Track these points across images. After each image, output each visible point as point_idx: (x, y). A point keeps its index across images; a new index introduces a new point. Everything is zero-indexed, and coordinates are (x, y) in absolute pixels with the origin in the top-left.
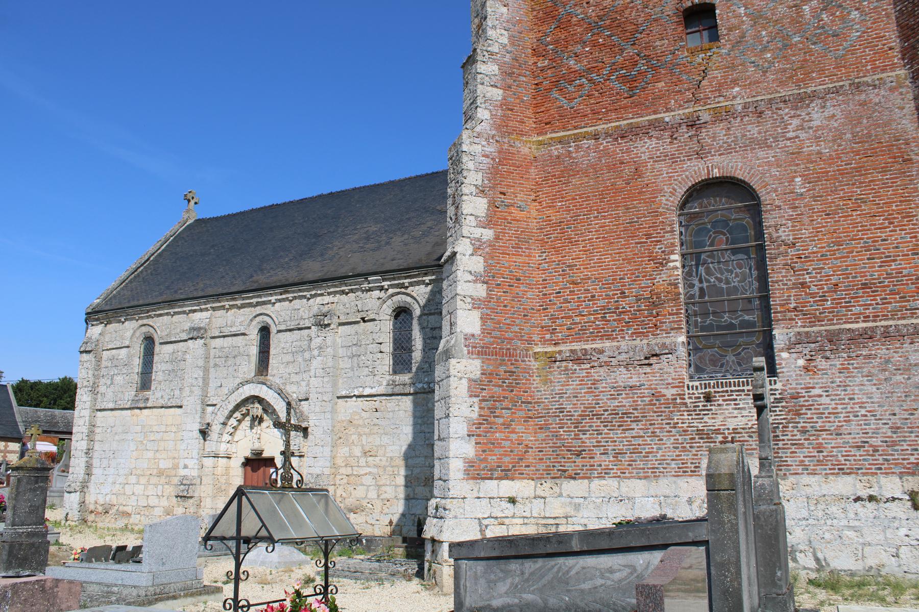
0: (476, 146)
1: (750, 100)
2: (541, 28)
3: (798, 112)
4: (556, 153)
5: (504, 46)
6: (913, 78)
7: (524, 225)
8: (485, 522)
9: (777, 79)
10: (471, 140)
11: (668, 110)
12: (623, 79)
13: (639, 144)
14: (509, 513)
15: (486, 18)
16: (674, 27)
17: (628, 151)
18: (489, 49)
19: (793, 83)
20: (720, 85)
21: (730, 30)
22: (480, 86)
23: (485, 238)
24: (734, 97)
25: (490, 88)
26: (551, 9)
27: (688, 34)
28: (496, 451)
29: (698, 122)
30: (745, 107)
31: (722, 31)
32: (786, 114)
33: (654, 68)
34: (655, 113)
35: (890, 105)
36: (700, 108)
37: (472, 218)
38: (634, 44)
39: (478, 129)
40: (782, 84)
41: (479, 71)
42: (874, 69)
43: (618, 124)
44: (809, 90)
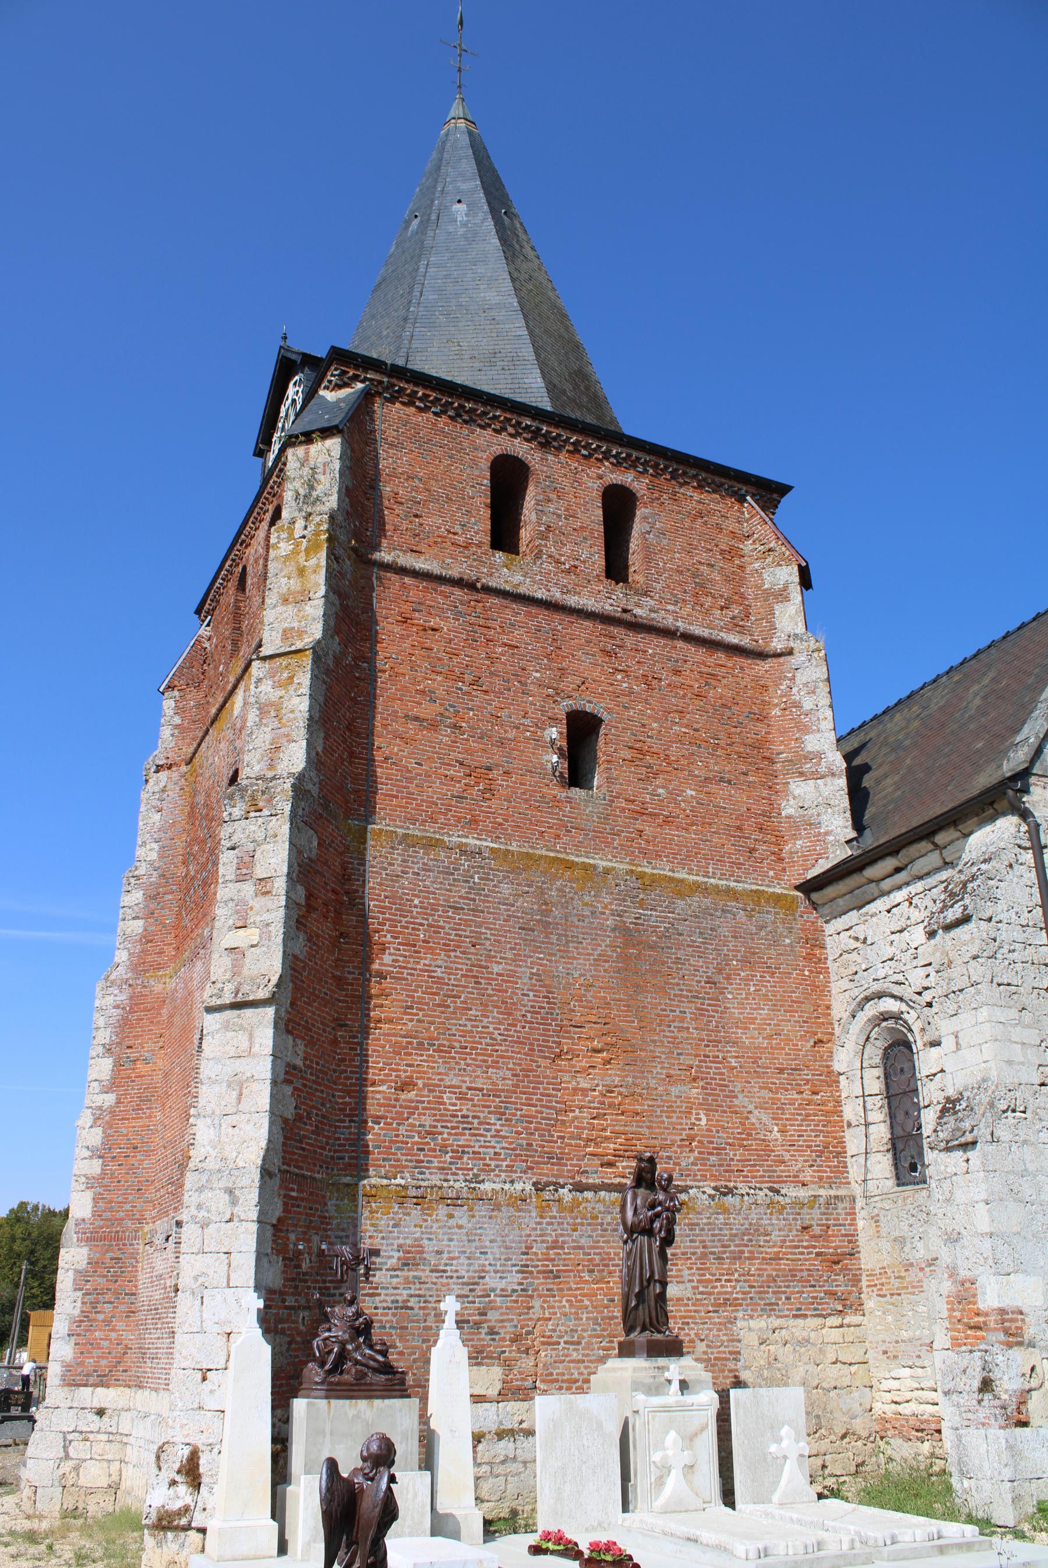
5: (151, 863)
7: (147, 1080)
8: (70, 1437)
14: (94, 1427)
23: (107, 1104)
28: (96, 1353)
37: (96, 1084)
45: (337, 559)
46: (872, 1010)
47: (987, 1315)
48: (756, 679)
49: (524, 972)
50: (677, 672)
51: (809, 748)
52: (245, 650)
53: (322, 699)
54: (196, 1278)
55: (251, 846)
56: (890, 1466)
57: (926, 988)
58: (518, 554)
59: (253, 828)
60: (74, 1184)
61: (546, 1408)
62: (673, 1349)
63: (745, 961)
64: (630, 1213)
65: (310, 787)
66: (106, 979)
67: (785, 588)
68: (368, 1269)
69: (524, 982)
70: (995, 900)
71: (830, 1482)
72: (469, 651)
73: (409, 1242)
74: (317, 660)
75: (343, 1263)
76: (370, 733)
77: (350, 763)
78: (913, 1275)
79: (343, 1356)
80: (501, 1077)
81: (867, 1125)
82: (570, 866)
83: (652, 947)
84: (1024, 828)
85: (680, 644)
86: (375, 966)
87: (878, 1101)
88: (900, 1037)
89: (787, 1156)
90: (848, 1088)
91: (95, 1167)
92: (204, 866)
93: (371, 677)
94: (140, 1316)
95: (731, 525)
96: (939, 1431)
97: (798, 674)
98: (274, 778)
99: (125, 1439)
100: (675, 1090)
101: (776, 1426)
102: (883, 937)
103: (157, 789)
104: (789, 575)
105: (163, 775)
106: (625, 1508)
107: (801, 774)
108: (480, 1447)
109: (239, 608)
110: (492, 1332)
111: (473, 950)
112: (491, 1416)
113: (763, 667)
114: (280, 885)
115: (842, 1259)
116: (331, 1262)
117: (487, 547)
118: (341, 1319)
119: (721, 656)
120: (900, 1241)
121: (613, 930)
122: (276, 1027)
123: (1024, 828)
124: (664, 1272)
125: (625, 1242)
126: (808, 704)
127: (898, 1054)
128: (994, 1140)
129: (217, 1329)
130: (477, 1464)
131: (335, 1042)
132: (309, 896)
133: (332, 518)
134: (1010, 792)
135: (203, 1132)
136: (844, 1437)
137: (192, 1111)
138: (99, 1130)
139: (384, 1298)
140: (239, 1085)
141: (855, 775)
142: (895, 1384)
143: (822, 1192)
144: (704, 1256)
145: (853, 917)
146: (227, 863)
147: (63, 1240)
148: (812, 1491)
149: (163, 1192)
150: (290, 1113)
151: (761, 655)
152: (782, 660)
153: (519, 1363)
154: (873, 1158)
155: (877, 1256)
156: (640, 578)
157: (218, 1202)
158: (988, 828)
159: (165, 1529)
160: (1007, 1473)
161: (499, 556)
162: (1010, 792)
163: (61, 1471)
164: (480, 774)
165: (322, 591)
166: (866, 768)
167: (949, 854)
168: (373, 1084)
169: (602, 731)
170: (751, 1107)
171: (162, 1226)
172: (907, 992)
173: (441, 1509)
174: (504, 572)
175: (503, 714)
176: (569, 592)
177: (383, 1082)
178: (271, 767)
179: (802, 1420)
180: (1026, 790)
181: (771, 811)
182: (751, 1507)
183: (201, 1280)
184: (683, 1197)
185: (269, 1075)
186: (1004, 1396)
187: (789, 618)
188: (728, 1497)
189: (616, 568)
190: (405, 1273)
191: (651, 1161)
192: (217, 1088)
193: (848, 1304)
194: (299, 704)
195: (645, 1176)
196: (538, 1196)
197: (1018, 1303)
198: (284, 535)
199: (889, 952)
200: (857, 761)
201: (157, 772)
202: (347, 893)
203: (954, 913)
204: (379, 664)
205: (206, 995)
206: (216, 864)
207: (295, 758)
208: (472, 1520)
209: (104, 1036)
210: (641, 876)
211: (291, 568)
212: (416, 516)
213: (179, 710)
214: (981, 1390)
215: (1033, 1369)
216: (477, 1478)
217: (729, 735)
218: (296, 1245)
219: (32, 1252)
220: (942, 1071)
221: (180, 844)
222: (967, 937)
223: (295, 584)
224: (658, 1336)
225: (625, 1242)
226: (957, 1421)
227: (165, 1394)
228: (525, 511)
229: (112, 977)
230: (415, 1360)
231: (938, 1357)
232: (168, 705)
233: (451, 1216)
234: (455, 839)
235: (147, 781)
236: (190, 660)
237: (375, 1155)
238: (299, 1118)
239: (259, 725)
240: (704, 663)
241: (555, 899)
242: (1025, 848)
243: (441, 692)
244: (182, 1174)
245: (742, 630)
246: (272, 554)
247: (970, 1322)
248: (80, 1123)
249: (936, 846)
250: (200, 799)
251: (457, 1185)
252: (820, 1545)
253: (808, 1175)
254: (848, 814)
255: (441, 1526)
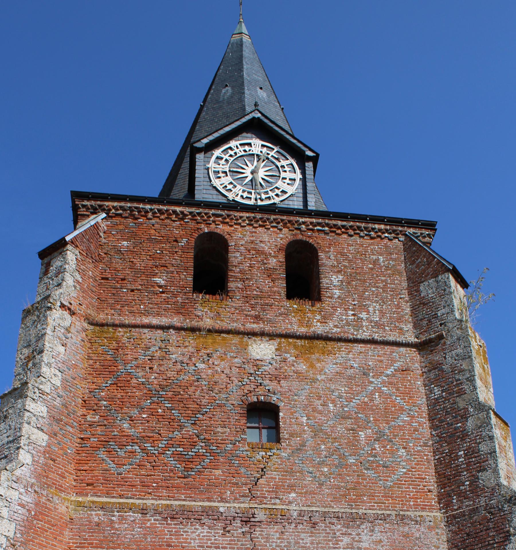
0: (13, 492)
1: (305, 508)
2: (95, 380)
3: (349, 531)
4: (96, 519)
6: (447, 522)
9: (332, 494)
10: (10, 484)
11: (223, 500)
12: (179, 457)
13: (189, 528)
15: (41, 352)
16: (237, 417)
17: (177, 534)
18: (41, 387)
19: (346, 501)
20: (277, 487)
21: (292, 435)
22: (25, 425)
24: (290, 503)
25: (36, 431)
26: (110, 363)
27: (248, 428)
29: (253, 520)
30: (300, 515)
31: (284, 434)
32: (338, 531)
33: (212, 453)
34: (209, 500)
35: (427, 542)
36: (256, 506)
38: (195, 424)
39: (18, 472)
40: (336, 500)
41: (27, 407)
42: (416, 505)
43: (168, 502)
44: (361, 512)
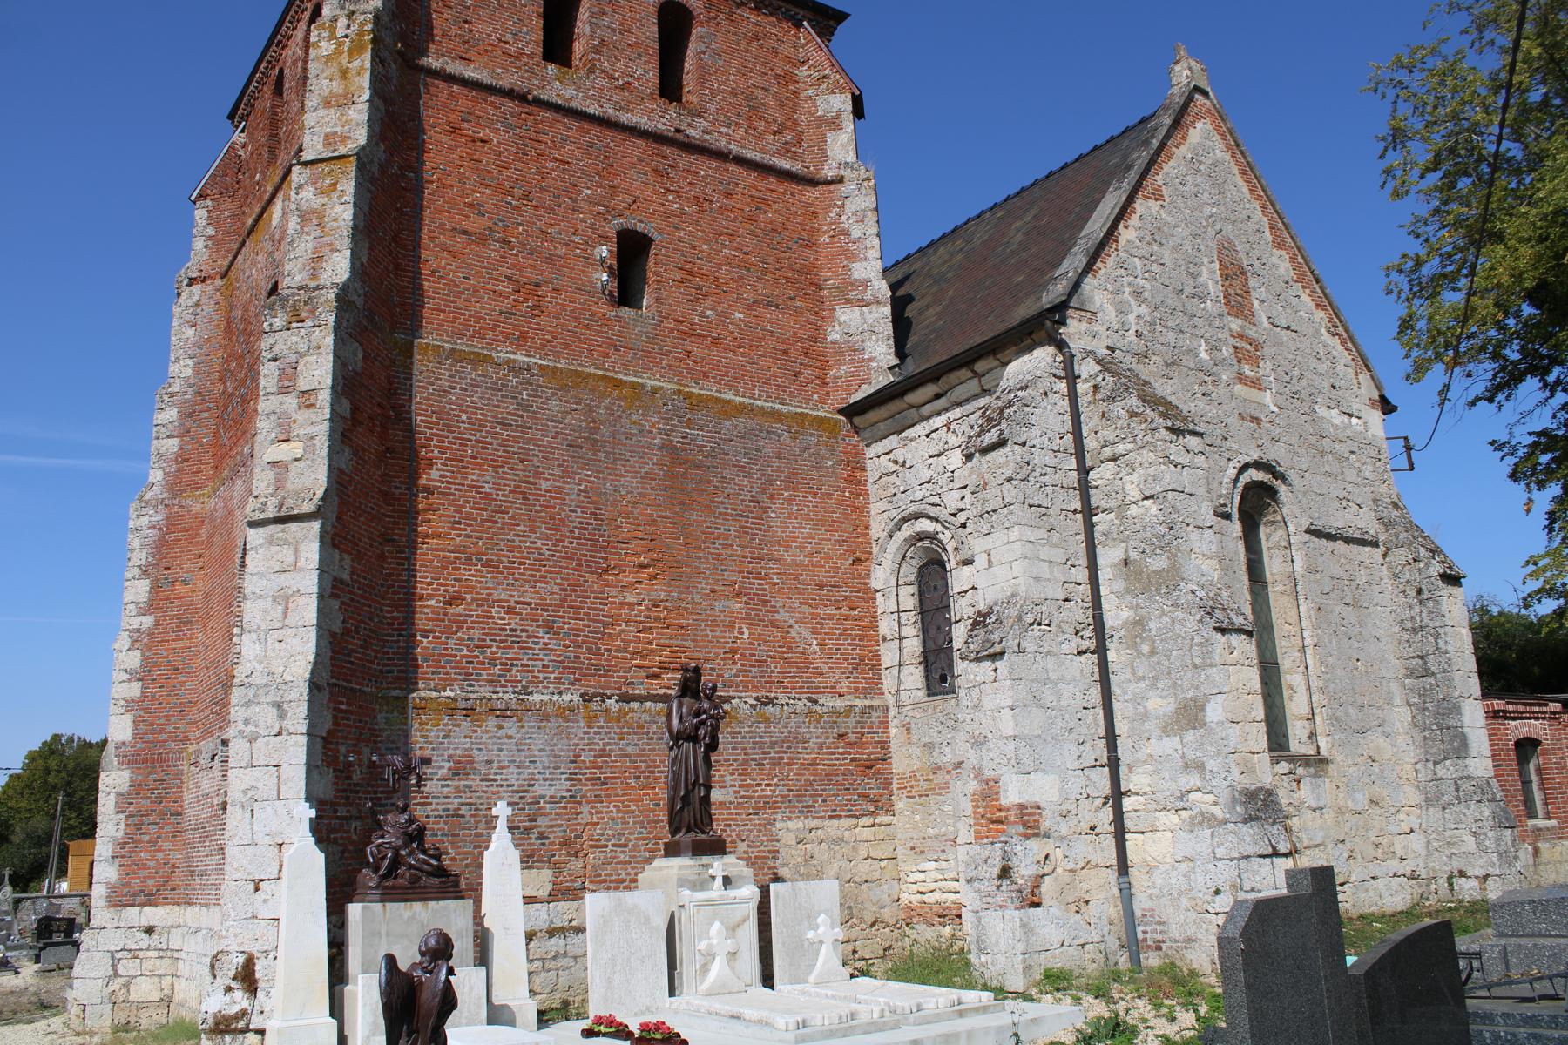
5: (186, 380)
7: (187, 601)
8: (118, 955)
14: (143, 945)
23: (145, 627)
28: (142, 873)
37: (132, 607)
45: (382, 62)
46: (907, 530)
47: (1008, 810)
48: (807, 205)
49: (572, 487)
50: (728, 195)
51: (856, 276)
52: (283, 159)
53: (366, 208)
54: (245, 792)
55: (293, 358)
56: (915, 948)
57: (961, 510)
58: (570, 67)
59: (295, 339)
60: (112, 707)
61: (595, 904)
62: (717, 847)
63: (789, 482)
64: (675, 721)
65: (355, 298)
66: (141, 499)
67: (838, 116)
68: (420, 778)
69: (571, 499)
70: (1030, 425)
71: (860, 964)
72: (519, 165)
73: (459, 752)
74: (361, 167)
75: (395, 772)
76: (416, 245)
77: (396, 275)
78: (940, 778)
79: (396, 862)
80: (549, 591)
81: (901, 639)
82: (619, 384)
83: (697, 467)
84: (1060, 358)
85: (732, 167)
86: (423, 481)
87: (912, 617)
88: (934, 556)
89: (825, 669)
90: (884, 604)
91: (135, 690)
92: (243, 381)
93: (418, 188)
94: (188, 835)
95: (786, 50)
96: (959, 916)
97: (847, 202)
98: (317, 288)
99: (176, 955)
100: (719, 605)
101: (813, 914)
102: (922, 462)
103: (190, 303)
104: (840, 103)
105: (197, 289)
106: (672, 993)
107: (848, 301)
108: (532, 945)
109: (276, 114)
110: (542, 837)
111: (520, 466)
112: (542, 915)
113: (813, 194)
114: (325, 397)
115: (875, 764)
116: (382, 773)
117: (538, 58)
118: (394, 826)
119: (772, 181)
120: (930, 746)
121: (660, 449)
122: (322, 541)
123: (1060, 358)
124: (708, 777)
125: (671, 749)
126: (856, 233)
127: (932, 574)
128: (1020, 650)
129: (268, 840)
130: (530, 961)
131: (382, 557)
132: (355, 409)
133: (377, 17)
134: (1048, 323)
135: (249, 648)
136: (873, 925)
137: (236, 631)
138: (138, 653)
139: (435, 807)
140: (284, 599)
141: (899, 305)
142: (921, 877)
143: (857, 702)
144: (745, 762)
145: (892, 441)
146: (268, 375)
147: (103, 764)
148: (848, 971)
149: (207, 712)
150: (337, 627)
151: (812, 182)
152: (832, 187)
153: (569, 865)
154: (907, 670)
155: (907, 761)
156: (694, 99)
157: (265, 716)
158: (1026, 358)
159: (222, 1032)
160: (1020, 947)
161: (551, 69)
162: (1048, 323)
163: (110, 989)
164: (528, 289)
165: (366, 95)
166: (909, 299)
167: (987, 382)
168: (421, 598)
169: (653, 251)
170: (792, 622)
171: (207, 746)
172: (943, 513)
173: (496, 1001)
174: (556, 86)
175: (553, 230)
176: (622, 109)
177: (431, 597)
178: (314, 277)
179: (837, 910)
180: (1063, 323)
181: (817, 336)
182: (789, 987)
183: (250, 793)
184: (726, 706)
185: (315, 589)
186: (1021, 881)
187: (841, 147)
188: (768, 980)
189: (670, 88)
190: (456, 783)
191: (697, 670)
192: (261, 603)
193: (881, 805)
194: (343, 213)
195: (691, 685)
196: (586, 707)
197: (1036, 799)
198: (326, 34)
199: (927, 474)
200: (901, 292)
201: (190, 284)
202: (393, 408)
203: (990, 437)
204: (427, 175)
205: (248, 511)
206: (255, 380)
207: (339, 267)
208: (527, 1009)
209: (140, 557)
210: (688, 396)
211: (333, 69)
212: (466, 22)
213: (212, 221)
214: (1000, 877)
215: (1047, 857)
216: (530, 973)
217: (778, 260)
218: (346, 757)
219: (69, 784)
220: (973, 588)
221: (216, 360)
222: (1002, 460)
223: (337, 86)
224: (704, 837)
225: (671, 749)
226: (977, 905)
227: (217, 909)
228: (579, 23)
229: (147, 497)
230: (467, 866)
231: (962, 852)
232: (201, 215)
233: (500, 727)
234: (503, 355)
235: (179, 295)
236: (224, 166)
237: (424, 667)
238: (346, 632)
239: (300, 233)
240: (755, 187)
241: (603, 418)
242: (1060, 378)
243: (490, 206)
244: (227, 694)
245: (794, 157)
246: (312, 53)
247: (993, 817)
248: (117, 646)
249: (975, 373)
250: (238, 313)
251: (506, 697)
252: (853, 1016)
253: (844, 686)
254: (891, 342)
255: (497, 1015)
